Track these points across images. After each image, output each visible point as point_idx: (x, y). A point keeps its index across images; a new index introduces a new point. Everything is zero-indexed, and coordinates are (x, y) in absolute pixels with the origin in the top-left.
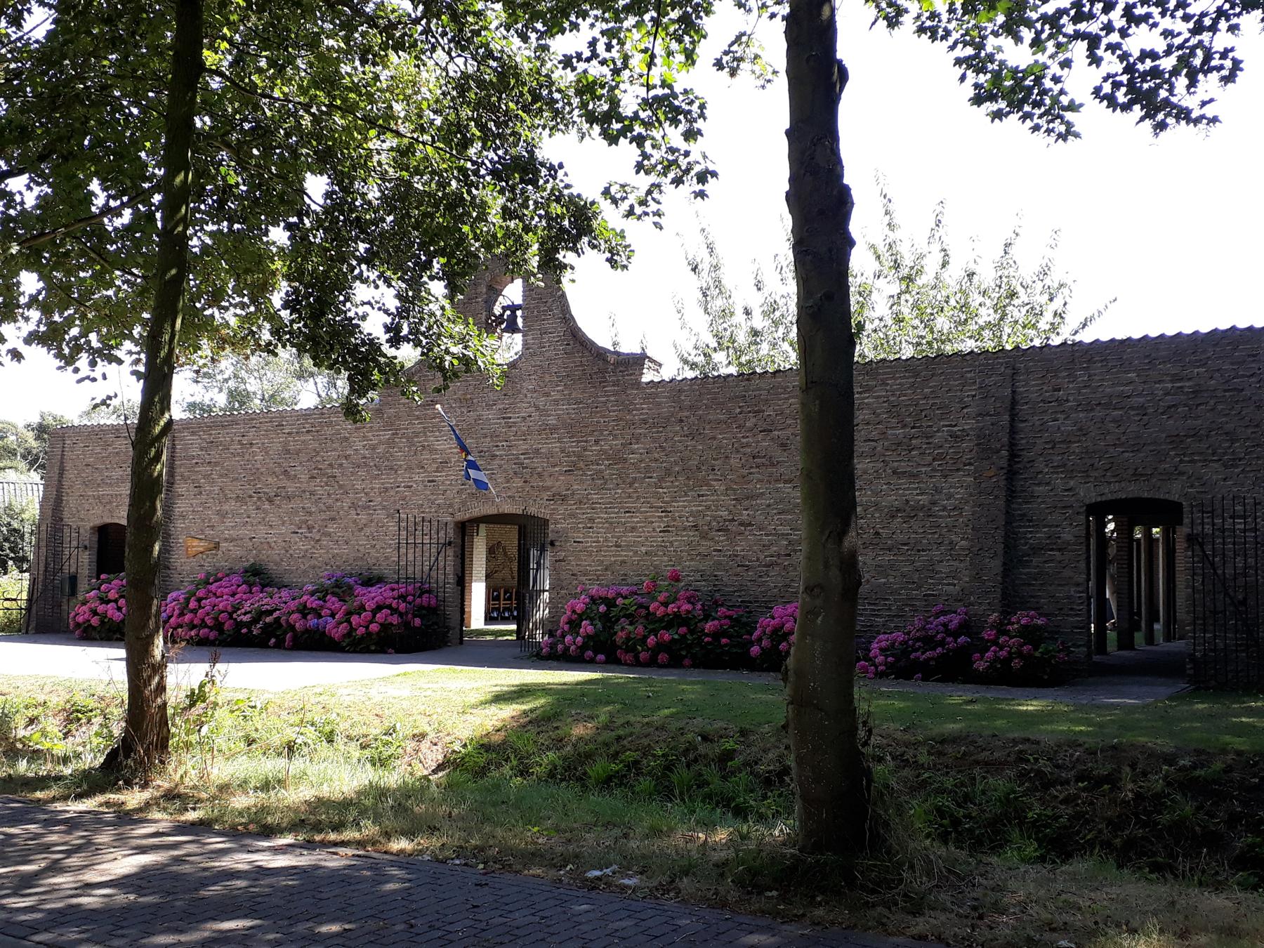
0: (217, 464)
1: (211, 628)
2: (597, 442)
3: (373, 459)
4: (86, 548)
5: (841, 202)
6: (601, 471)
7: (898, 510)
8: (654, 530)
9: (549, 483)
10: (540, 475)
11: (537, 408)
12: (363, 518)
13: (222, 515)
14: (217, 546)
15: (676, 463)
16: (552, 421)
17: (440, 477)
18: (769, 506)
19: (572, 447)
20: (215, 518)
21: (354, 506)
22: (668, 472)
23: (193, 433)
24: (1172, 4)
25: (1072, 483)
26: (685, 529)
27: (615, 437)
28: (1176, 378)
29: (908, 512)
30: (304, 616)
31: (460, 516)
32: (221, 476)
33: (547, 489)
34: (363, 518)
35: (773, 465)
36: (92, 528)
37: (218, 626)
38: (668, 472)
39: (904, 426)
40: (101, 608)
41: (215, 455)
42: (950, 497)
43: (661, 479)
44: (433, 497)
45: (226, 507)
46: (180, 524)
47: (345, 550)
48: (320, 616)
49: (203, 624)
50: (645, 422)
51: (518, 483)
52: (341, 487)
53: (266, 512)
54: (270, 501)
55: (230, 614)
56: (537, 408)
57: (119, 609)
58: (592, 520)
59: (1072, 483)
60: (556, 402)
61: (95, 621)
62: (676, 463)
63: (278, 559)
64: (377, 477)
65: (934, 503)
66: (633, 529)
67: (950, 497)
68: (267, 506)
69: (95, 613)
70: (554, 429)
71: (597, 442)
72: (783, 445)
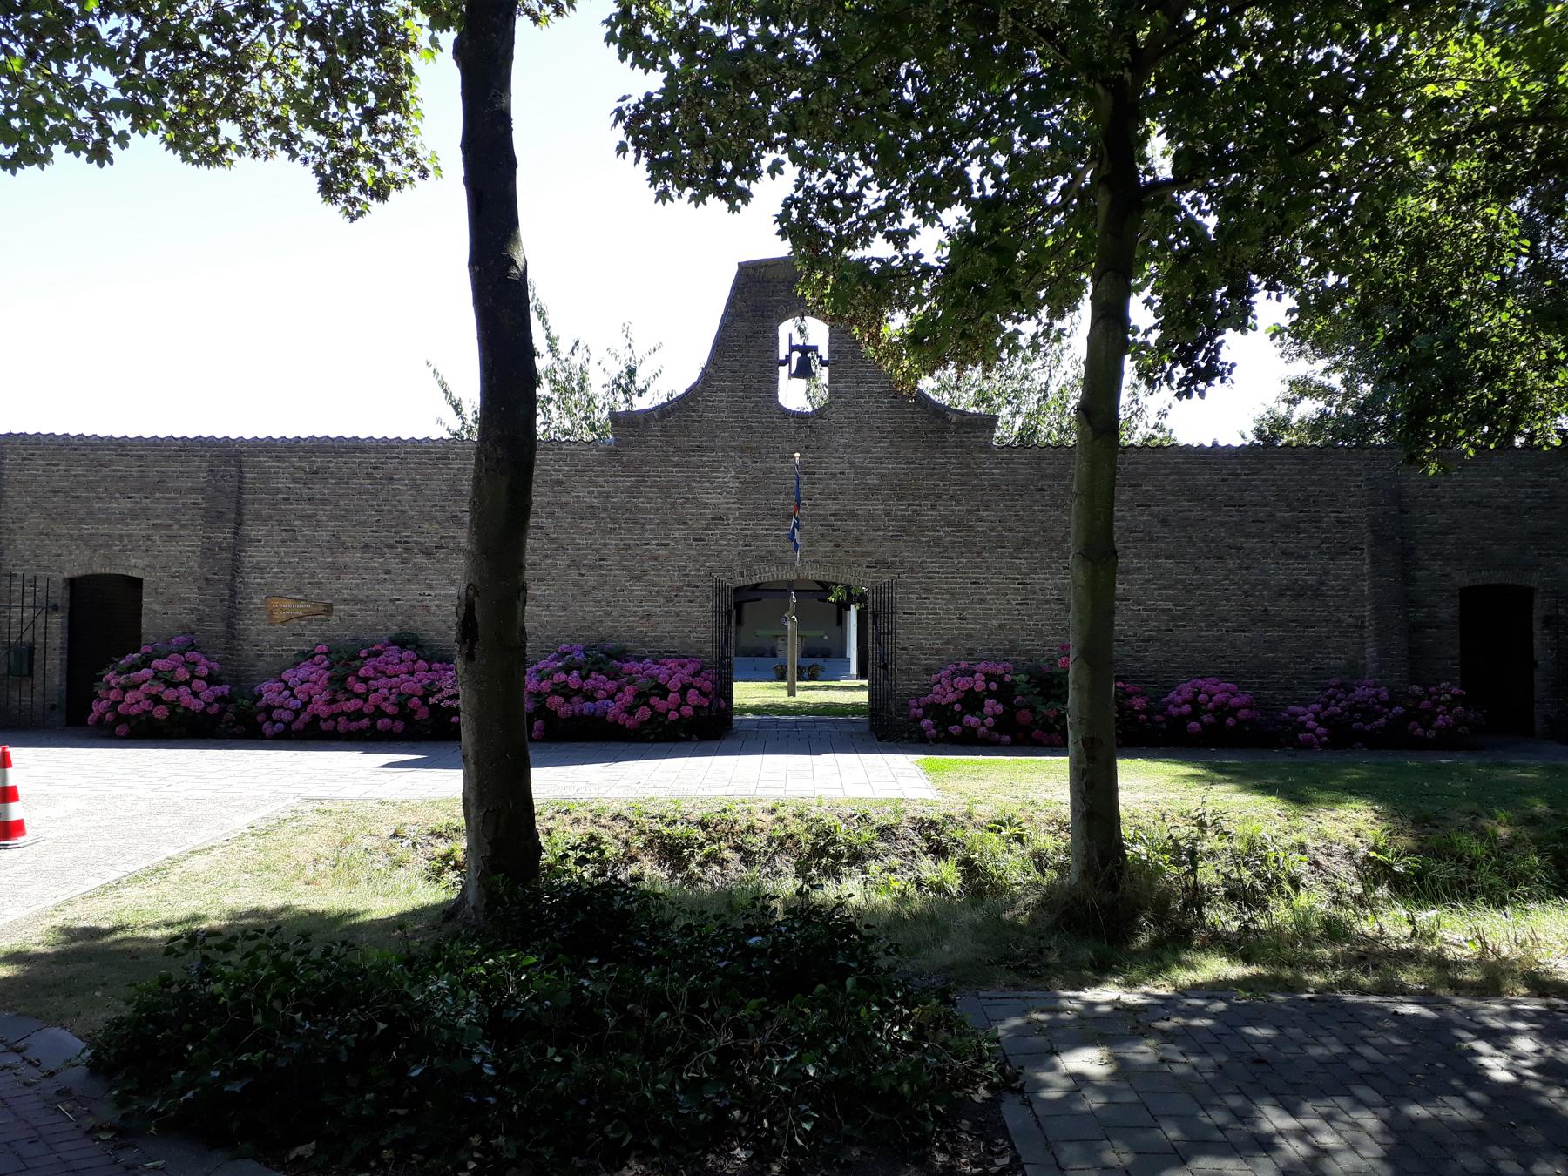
0: (324, 502)
1: (394, 718)
2: (934, 507)
3: (605, 509)
4: (56, 608)
5: (509, 164)
6: (940, 538)
7: (1288, 589)
8: (1009, 603)
9: (870, 549)
10: (856, 539)
11: (852, 464)
12: (591, 579)
13: (338, 570)
14: (328, 610)
15: (1037, 534)
16: (873, 480)
17: (710, 535)
18: (1148, 581)
19: (899, 508)
20: (322, 574)
21: (574, 564)
22: (1027, 542)
23: (279, 459)
24: (933, 3)
25: (1448, 569)
26: (1048, 602)
27: (959, 502)
28: (1535, 485)
29: (1298, 591)
30: (567, 699)
31: (742, 581)
32: (333, 517)
33: (868, 554)
34: (591, 579)
35: (1151, 540)
36: (65, 580)
37: (404, 713)
38: (1027, 542)
39: (1293, 510)
40: (169, 694)
41: (320, 490)
42: (1337, 577)
43: (1018, 549)
44: (702, 559)
45: (345, 559)
46: (254, 580)
47: (561, 617)
48: (595, 700)
49: (379, 712)
50: (996, 488)
51: (825, 547)
52: (552, 540)
53: (421, 569)
54: (428, 553)
55: (424, 699)
56: (852, 464)
57: (196, 694)
58: (926, 590)
59: (1448, 569)
60: (879, 460)
61: (160, 713)
62: (1037, 534)
63: (444, 628)
64: (605, 532)
65: (1322, 583)
66: (982, 601)
67: (1337, 577)
68: (421, 559)
69: (157, 700)
70: (874, 490)
71: (934, 507)
72: (1164, 521)
